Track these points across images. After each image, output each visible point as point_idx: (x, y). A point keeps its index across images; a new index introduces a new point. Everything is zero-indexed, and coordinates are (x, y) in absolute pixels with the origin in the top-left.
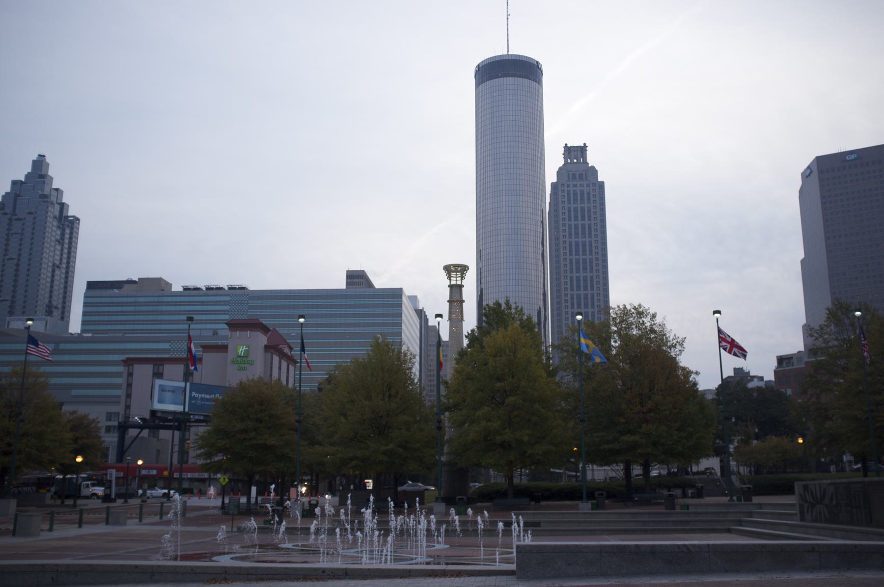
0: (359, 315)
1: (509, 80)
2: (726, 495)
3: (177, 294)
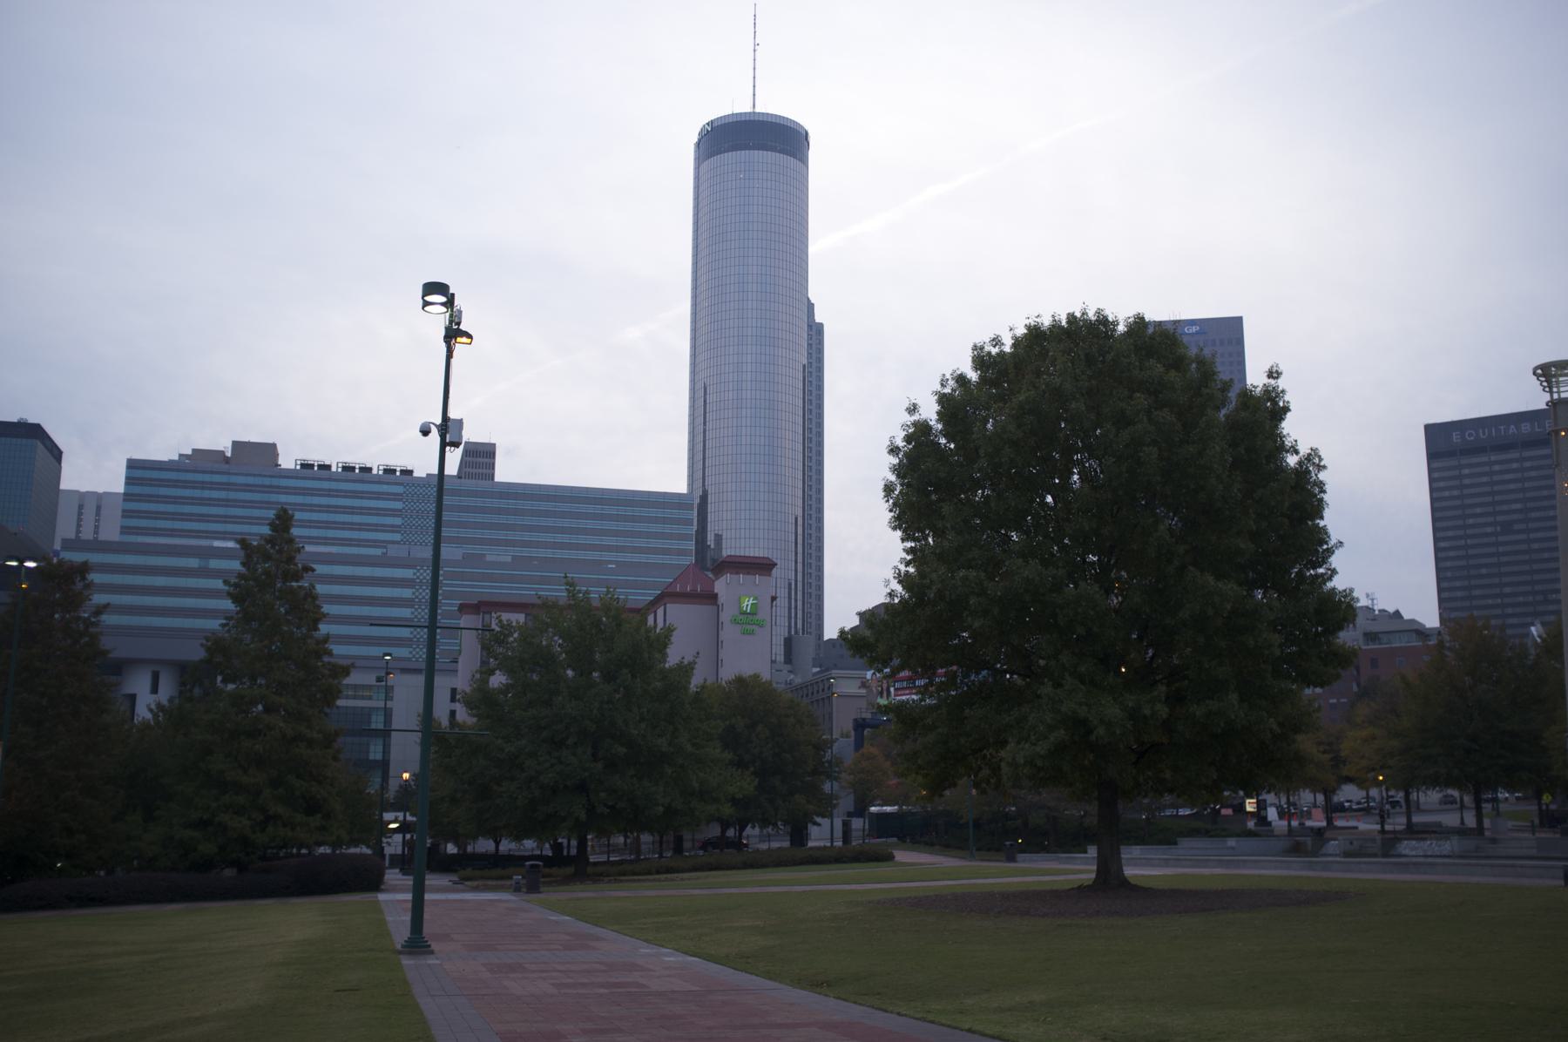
0: (562, 530)
1: (752, 156)
2: (1066, 840)
3: (288, 474)
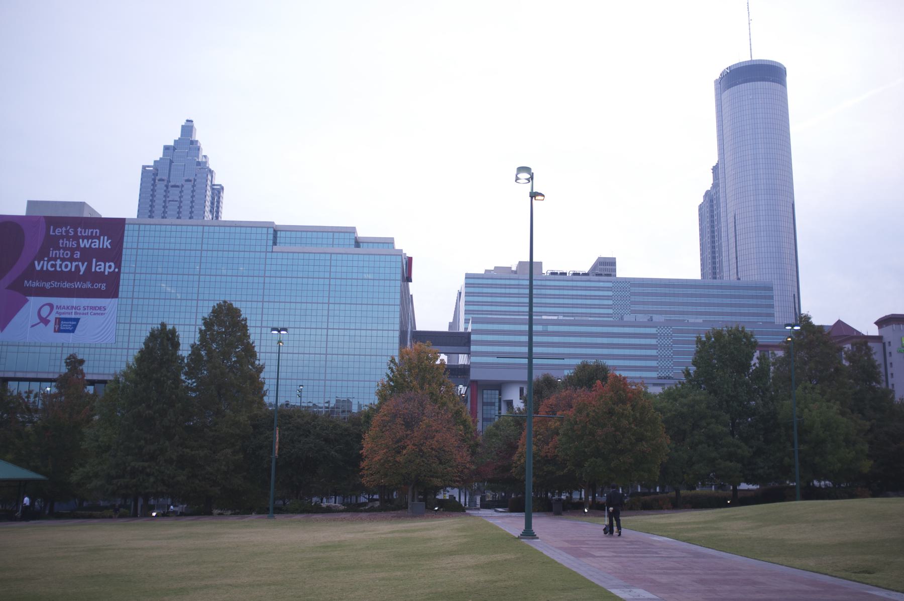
1: (754, 84)
